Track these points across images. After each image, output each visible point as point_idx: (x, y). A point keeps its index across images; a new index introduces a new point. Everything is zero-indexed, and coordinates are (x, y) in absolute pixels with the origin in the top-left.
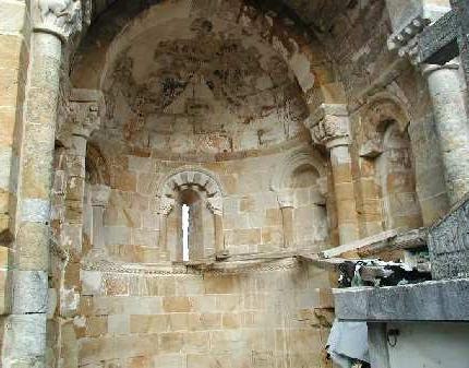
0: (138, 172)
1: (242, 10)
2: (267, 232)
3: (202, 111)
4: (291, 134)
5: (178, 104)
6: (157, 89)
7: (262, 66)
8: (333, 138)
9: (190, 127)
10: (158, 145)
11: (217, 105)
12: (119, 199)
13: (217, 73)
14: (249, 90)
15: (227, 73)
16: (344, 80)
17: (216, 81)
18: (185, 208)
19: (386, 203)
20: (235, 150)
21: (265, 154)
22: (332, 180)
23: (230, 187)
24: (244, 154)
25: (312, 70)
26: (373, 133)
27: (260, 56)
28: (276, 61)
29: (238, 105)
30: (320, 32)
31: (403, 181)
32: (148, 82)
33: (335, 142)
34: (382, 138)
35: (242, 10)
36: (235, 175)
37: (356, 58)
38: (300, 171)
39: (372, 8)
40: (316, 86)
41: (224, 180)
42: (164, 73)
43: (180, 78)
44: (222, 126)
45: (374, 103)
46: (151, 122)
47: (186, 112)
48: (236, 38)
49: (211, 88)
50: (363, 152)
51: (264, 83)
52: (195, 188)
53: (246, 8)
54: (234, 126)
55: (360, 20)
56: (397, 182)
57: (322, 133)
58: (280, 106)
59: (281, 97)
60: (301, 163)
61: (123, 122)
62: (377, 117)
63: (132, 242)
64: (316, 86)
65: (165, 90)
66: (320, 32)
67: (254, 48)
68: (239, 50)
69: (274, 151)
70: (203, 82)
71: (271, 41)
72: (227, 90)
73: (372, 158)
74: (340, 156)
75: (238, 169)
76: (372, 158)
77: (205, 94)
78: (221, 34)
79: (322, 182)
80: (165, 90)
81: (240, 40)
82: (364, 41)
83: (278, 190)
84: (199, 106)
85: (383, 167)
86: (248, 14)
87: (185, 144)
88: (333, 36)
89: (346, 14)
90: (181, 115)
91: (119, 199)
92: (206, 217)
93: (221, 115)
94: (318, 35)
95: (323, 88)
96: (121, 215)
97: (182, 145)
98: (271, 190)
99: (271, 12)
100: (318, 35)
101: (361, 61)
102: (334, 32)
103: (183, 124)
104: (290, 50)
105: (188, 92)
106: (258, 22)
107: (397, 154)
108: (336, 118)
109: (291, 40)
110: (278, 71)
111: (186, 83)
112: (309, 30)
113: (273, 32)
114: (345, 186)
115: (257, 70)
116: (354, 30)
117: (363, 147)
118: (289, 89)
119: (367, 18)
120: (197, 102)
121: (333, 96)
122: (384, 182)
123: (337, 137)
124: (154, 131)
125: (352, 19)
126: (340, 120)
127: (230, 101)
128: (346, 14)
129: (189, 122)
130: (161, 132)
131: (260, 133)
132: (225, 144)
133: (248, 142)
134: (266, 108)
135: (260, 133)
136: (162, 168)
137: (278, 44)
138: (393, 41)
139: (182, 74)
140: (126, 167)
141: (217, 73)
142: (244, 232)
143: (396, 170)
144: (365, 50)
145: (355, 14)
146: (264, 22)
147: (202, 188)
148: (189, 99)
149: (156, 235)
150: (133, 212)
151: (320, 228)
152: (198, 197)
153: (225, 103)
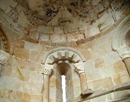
0: (30, 50)
2: (117, 77)
3: (68, 23)
5: (55, 21)
6: (43, 13)
9: (61, 32)
10: (45, 39)
11: (75, 20)
12: (14, 61)
13: (72, 4)
14: (89, 8)
15: (77, 3)
17: (72, 7)
18: (63, 77)
20: (86, 37)
21: (105, 33)
23: (88, 57)
24: (92, 38)
29: (85, 17)
32: (38, 9)
36: (89, 50)
41: (83, 53)
42: (46, 6)
43: (54, 9)
44: (79, 28)
46: (41, 29)
47: (59, 24)
49: (70, 12)
52: (67, 62)
54: (85, 27)
58: (107, 8)
61: (23, 25)
63: (21, 90)
65: (47, 14)
69: (109, 30)
70: (66, 9)
72: (79, 11)
75: (90, 46)
77: (68, 15)
80: (47, 14)
83: (118, 49)
84: (66, 22)
87: (59, 39)
90: (57, 26)
91: (14, 61)
92: (75, 77)
93: (77, 23)
96: (14, 71)
97: (58, 39)
98: (113, 50)
103: (58, 30)
105: (59, 15)
111: (57, 11)
120: (64, 19)
124: (42, 33)
127: (81, 16)
129: (61, 29)
130: (47, 34)
131: (99, 26)
132: (81, 37)
133: (94, 31)
135: (99, 26)
136: (46, 49)
139: (55, 6)
140: (23, 47)
141: (72, 4)
142: (100, 80)
147: (71, 61)
148: (59, 18)
149: (40, 87)
150: (23, 72)
152: (69, 67)
153: (78, 17)
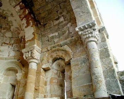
1: (19, 3)
4: (11, 55)
7: (11, 29)
8: (34, 59)
16: (42, 42)
19: (48, 87)
22: (26, 75)
25: (34, 34)
26: (51, 61)
27: (12, 25)
28: (16, 29)
30: (40, 24)
31: (56, 81)
33: (33, 60)
34: (52, 64)
35: (19, 3)
37: (51, 35)
38: (10, 69)
39: (64, 22)
40: (33, 39)
45: (55, 51)
48: (7, 15)
50: (44, 67)
51: (9, 34)
53: (21, 4)
55: (59, 24)
56: (54, 81)
57: (30, 55)
58: (10, 45)
59: (13, 42)
60: (14, 67)
62: (55, 55)
64: (33, 39)
66: (40, 24)
67: (12, 22)
68: (6, 20)
71: (22, 20)
73: (46, 70)
74: (33, 66)
76: (46, 70)
78: (4, 10)
79: (19, 76)
81: (8, 17)
82: (56, 31)
85: (50, 75)
86: (20, 6)
88: (44, 27)
89: (53, 22)
94: (39, 25)
95: (36, 40)
99: (28, 9)
100: (39, 25)
101: (53, 38)
102: (46, 26)
104: (28, 24)
106: (22, 11)
107: (56, 71)
108: (37, 53)
109: (30, 21)
110: (16, 33)
112: (39, 21)
113: (25, 17)
114: (32, 77)
115: (9, 29)
116: (54, 27)
117: (44, 65)
118: (17, 40)
119: (61, 24)
121: (38, 44)
122: (49, 80)
123: (35, 59)
125: (55, 24)
126: (38, 53)
128: (53, 22)
134: (5, 43)
137: (24, 21)
138: (78, 29)
143: (55, 77)
144: (57, 34)
145: (57, 22)
146: (25, 11)
151: (9, 94)
